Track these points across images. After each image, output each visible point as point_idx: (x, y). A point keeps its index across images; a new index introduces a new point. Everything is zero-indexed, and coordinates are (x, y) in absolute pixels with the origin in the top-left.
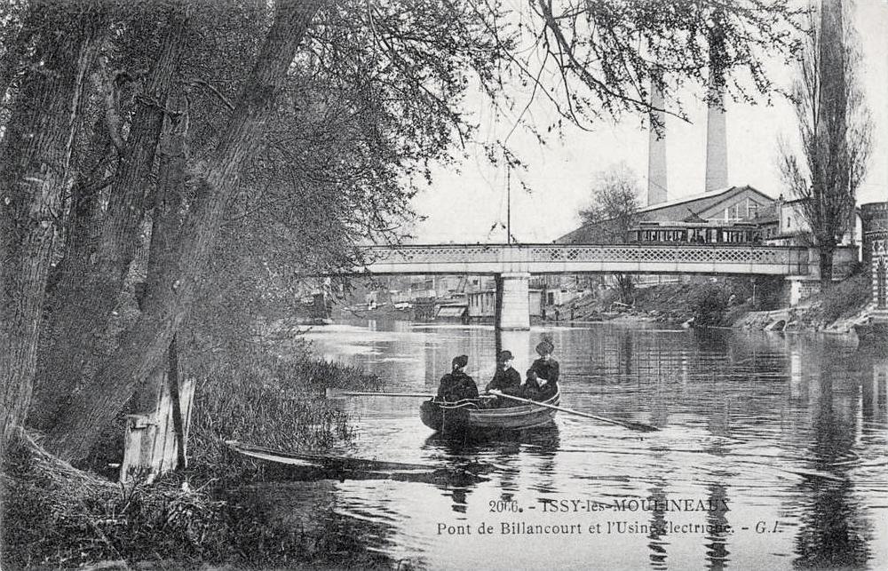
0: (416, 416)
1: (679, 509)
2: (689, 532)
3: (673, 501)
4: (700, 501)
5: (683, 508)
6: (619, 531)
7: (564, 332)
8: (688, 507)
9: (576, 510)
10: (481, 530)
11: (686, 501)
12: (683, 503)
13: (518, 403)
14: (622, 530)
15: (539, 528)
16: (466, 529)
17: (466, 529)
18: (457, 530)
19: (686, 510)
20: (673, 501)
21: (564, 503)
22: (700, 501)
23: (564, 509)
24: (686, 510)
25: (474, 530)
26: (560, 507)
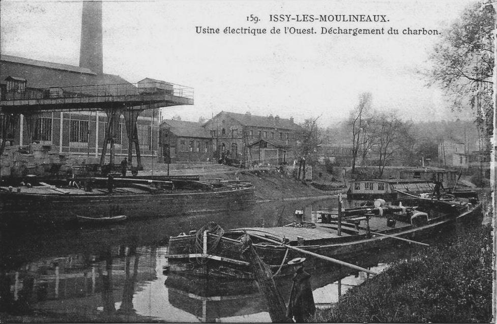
0: (317, 304)
1: (357, 20)
2: (228, 33)
3: (354, 16)
4: (369, 16)
5: (359, 19)
6: (197, 31)
7: (101, 119)
8: (305, 19)
9: (288, 21)
10: (273, 31)
11: (361, 16)
12: (359, 17)
13: (382, 236)
14: (199, 31)
15: (212, 30)
16: (381, 31)
17: (381, 31)
18: (261, 31)
19: (361, 21)
20: (354, 16)
21: (282, 16)
22: (369, 16)
23: (282, 20)
24: (361, 21)
25: (385, 31)
26: (279, 18)
